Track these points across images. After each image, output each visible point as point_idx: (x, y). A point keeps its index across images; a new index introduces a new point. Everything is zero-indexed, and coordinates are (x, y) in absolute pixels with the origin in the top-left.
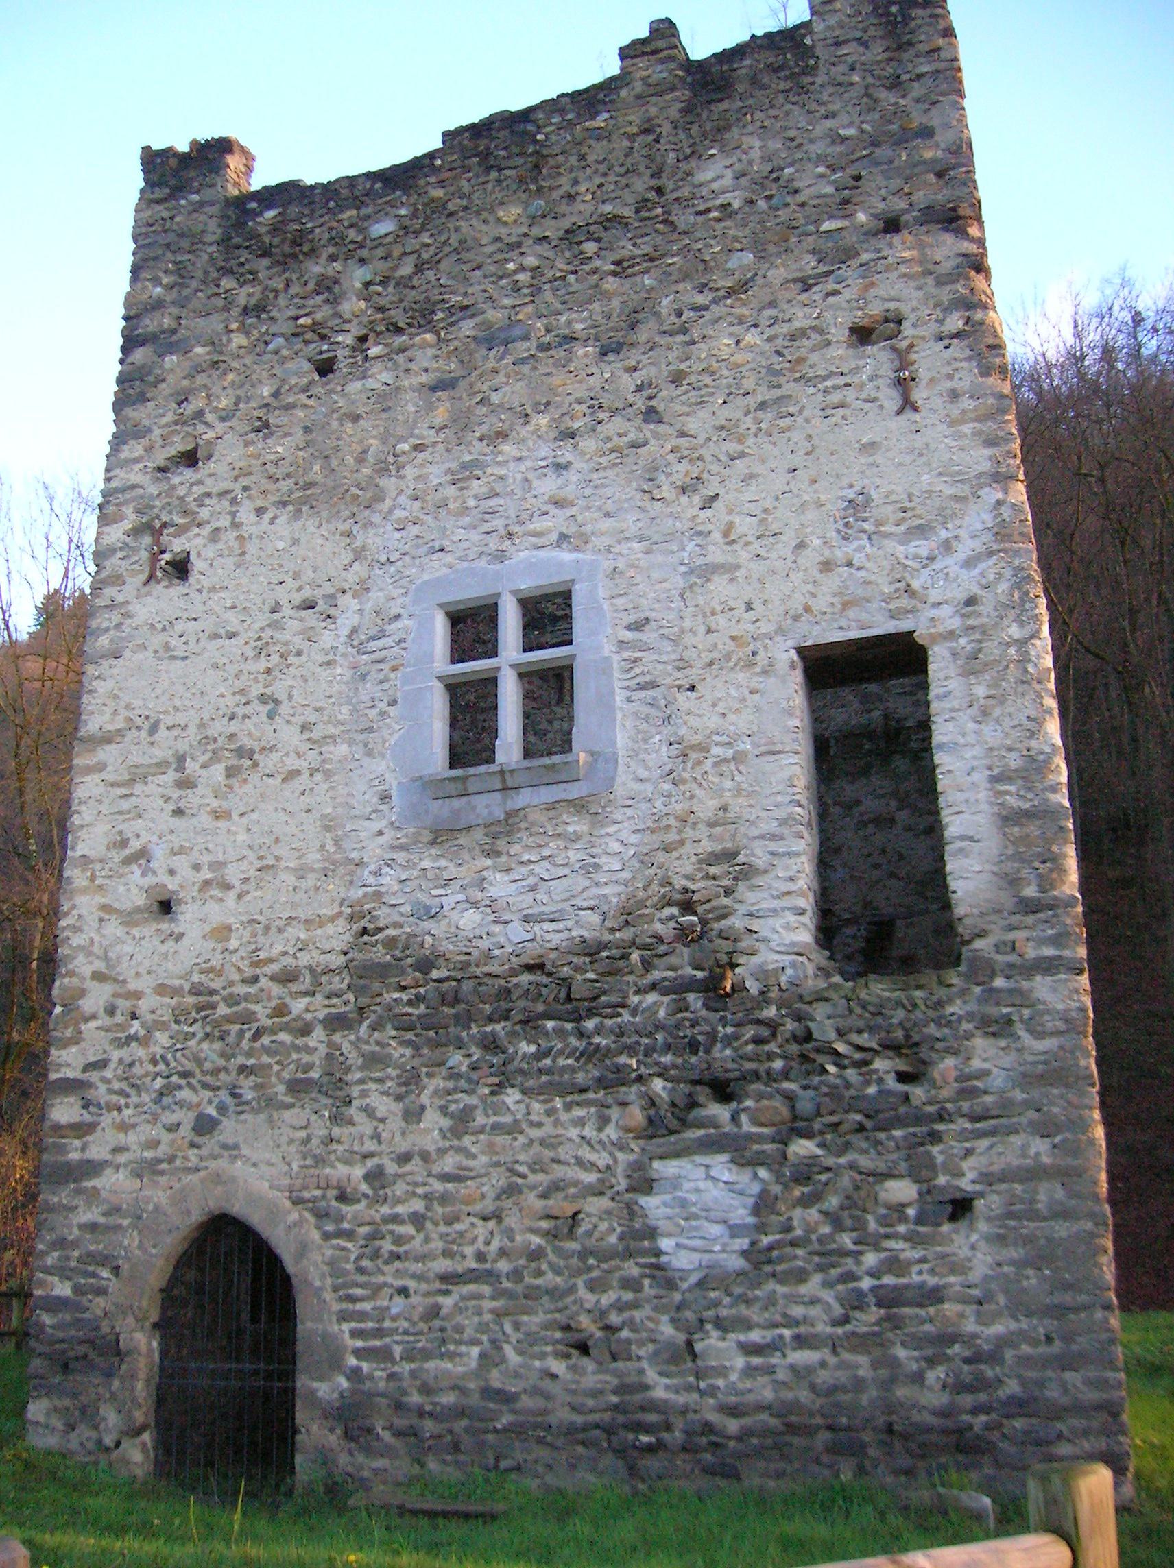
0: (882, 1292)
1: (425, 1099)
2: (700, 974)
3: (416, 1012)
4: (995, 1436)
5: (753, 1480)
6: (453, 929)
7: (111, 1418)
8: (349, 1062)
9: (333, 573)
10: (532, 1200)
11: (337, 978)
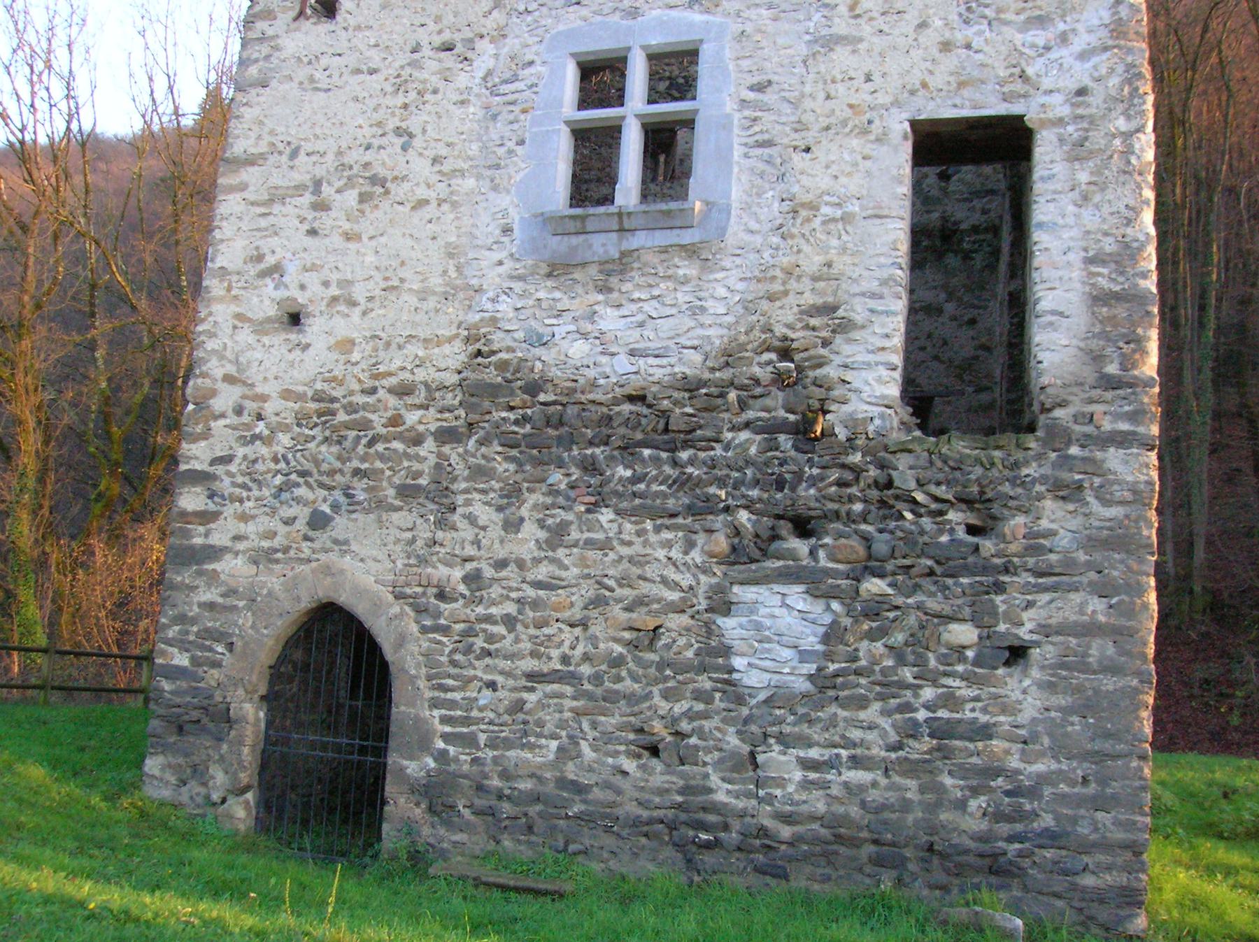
0: (936, 724)
1: (524, 512)
2: (792, 417)
3: (522, 431)
4: (1026, 863)
5: (799, 882)
6: (563, 357)
7: (219, 777)
8: (456, 473)
9: (472, 19)
10: (616, 611)
11: (451, 395)
